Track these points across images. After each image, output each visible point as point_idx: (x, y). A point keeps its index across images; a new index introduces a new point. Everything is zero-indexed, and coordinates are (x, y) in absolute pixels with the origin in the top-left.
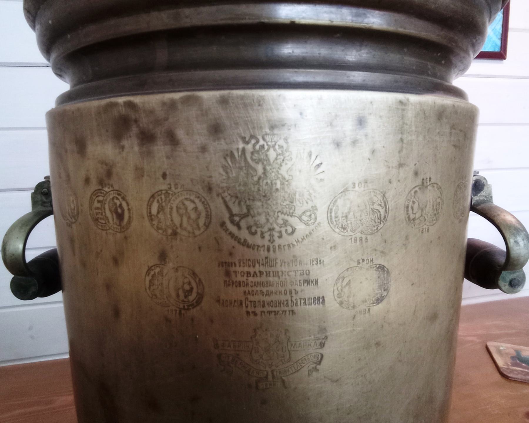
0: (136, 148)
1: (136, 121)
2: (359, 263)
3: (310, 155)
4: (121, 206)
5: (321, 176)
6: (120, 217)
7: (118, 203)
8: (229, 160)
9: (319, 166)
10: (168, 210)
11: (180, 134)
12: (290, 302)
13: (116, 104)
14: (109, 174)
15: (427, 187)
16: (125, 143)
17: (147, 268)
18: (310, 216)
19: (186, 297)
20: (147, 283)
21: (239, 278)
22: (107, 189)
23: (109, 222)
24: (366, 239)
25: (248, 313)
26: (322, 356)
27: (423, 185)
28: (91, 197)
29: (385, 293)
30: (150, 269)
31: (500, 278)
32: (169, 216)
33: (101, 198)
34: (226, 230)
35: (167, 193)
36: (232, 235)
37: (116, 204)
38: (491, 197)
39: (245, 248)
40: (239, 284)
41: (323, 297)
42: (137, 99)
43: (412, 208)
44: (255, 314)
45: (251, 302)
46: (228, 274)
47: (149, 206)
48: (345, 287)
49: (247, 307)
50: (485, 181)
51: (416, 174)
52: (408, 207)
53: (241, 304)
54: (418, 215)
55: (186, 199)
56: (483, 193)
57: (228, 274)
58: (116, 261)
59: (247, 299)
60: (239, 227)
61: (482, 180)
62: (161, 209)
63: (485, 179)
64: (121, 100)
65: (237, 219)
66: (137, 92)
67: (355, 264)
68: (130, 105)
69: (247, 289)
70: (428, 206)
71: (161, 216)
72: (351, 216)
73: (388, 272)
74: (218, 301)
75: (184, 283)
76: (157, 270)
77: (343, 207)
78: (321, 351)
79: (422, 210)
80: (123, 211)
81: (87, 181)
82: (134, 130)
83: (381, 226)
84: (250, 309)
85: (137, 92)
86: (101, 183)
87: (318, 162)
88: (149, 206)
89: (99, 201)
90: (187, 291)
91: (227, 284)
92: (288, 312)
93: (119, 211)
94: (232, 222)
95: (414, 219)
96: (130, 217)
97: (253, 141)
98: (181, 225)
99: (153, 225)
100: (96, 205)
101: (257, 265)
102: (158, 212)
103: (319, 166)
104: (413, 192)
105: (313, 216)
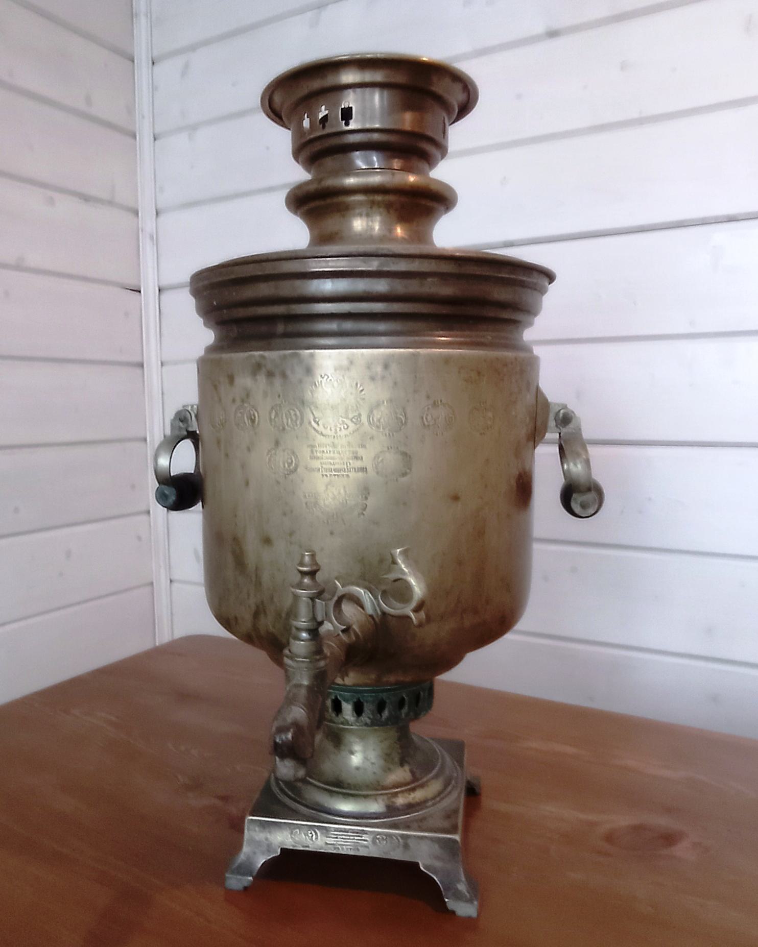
0: (264, 381)
1: (265, 366)
2: (388, 449)
3: (357, 384)
4: (254, 415)
5: (364, 397)
6: (253, 421)
7: (252, 413)
8: (313, 387)
9: (362, 391)
10: (280, 415)
11: (288, 372)
12: (346, 469)
13: (253, 356)
14: (248, 395)
15: (438, 406)
16: (258, 377)
17: (267, 451)
18: (357, 419)
19: (289, 466)
20: (267, 460)
21: (319, 455)
22: (246, 405)
23: (246, 425)
24: (393, 434)
25: (323, 475)
26: (366, 505)
27: (435, 404)
28: (236, 411)
29: (408, 471)
30: (269, 451)
31: (572, 500)
32: (281, 419)
33: (242, 411)
34: (312, 426)
35: (280, 406)
36: (315, 429)
37: (250, 414)
38: (580, 429)
39: (322, 437)
40: (318, 458)
41: (366, 469)
42: (266, 354)
43: (426, 419)
44: (326, 475)
45: (324, 468)
46: (312, 452)
47: (270, 413)
48: (380, 462)
49: (322, 472)
50: (573, 414)
51: (428, 397)
52: (422, 418)
53: (319, 470)
54: (431, 423)
55: (291, 409)
56: (571, 426)
57: (312, 452)
58: (249, 449)
59: (322, 467)
60: (318, 425)
61: (570, 413)
62: (277, 415)
63: (573, 412)
64: (257, 353)
65: (317, 420)
66: (286, 790)
67: (386, 449)
68: (263, 357)
69: (322, 461)
70: (440, 419)
71: (277, 419)
72: (382, 420)
73: (410, 457)
74: (306, 468)
75: (288, 459)
76: (273, 452)
77: (377, 415)
78: (365, 502)
79: (435, 420)
80: (255, 417)
81: (234, 401)
82: (264, 370)
83: (403, 427)
84: (324, 473)
85: (286, 790)
86: (243, 401)
87: (361, 388)
88: (270, 413)
89: (241, 413)
90: (290, 463)
91: (311, 458)
92: (345, 476)
93: (253, 417)
94: (315, 421)
95: (429, 426)
96: (259, 421)
97: (326, 377)
98: (287, 424)
99: (271, 424)
100: (239, 415)
101: (328, 447)
102: (275, 417)
103: (362, 391)
104: (426, 408)
105: (359, 419)
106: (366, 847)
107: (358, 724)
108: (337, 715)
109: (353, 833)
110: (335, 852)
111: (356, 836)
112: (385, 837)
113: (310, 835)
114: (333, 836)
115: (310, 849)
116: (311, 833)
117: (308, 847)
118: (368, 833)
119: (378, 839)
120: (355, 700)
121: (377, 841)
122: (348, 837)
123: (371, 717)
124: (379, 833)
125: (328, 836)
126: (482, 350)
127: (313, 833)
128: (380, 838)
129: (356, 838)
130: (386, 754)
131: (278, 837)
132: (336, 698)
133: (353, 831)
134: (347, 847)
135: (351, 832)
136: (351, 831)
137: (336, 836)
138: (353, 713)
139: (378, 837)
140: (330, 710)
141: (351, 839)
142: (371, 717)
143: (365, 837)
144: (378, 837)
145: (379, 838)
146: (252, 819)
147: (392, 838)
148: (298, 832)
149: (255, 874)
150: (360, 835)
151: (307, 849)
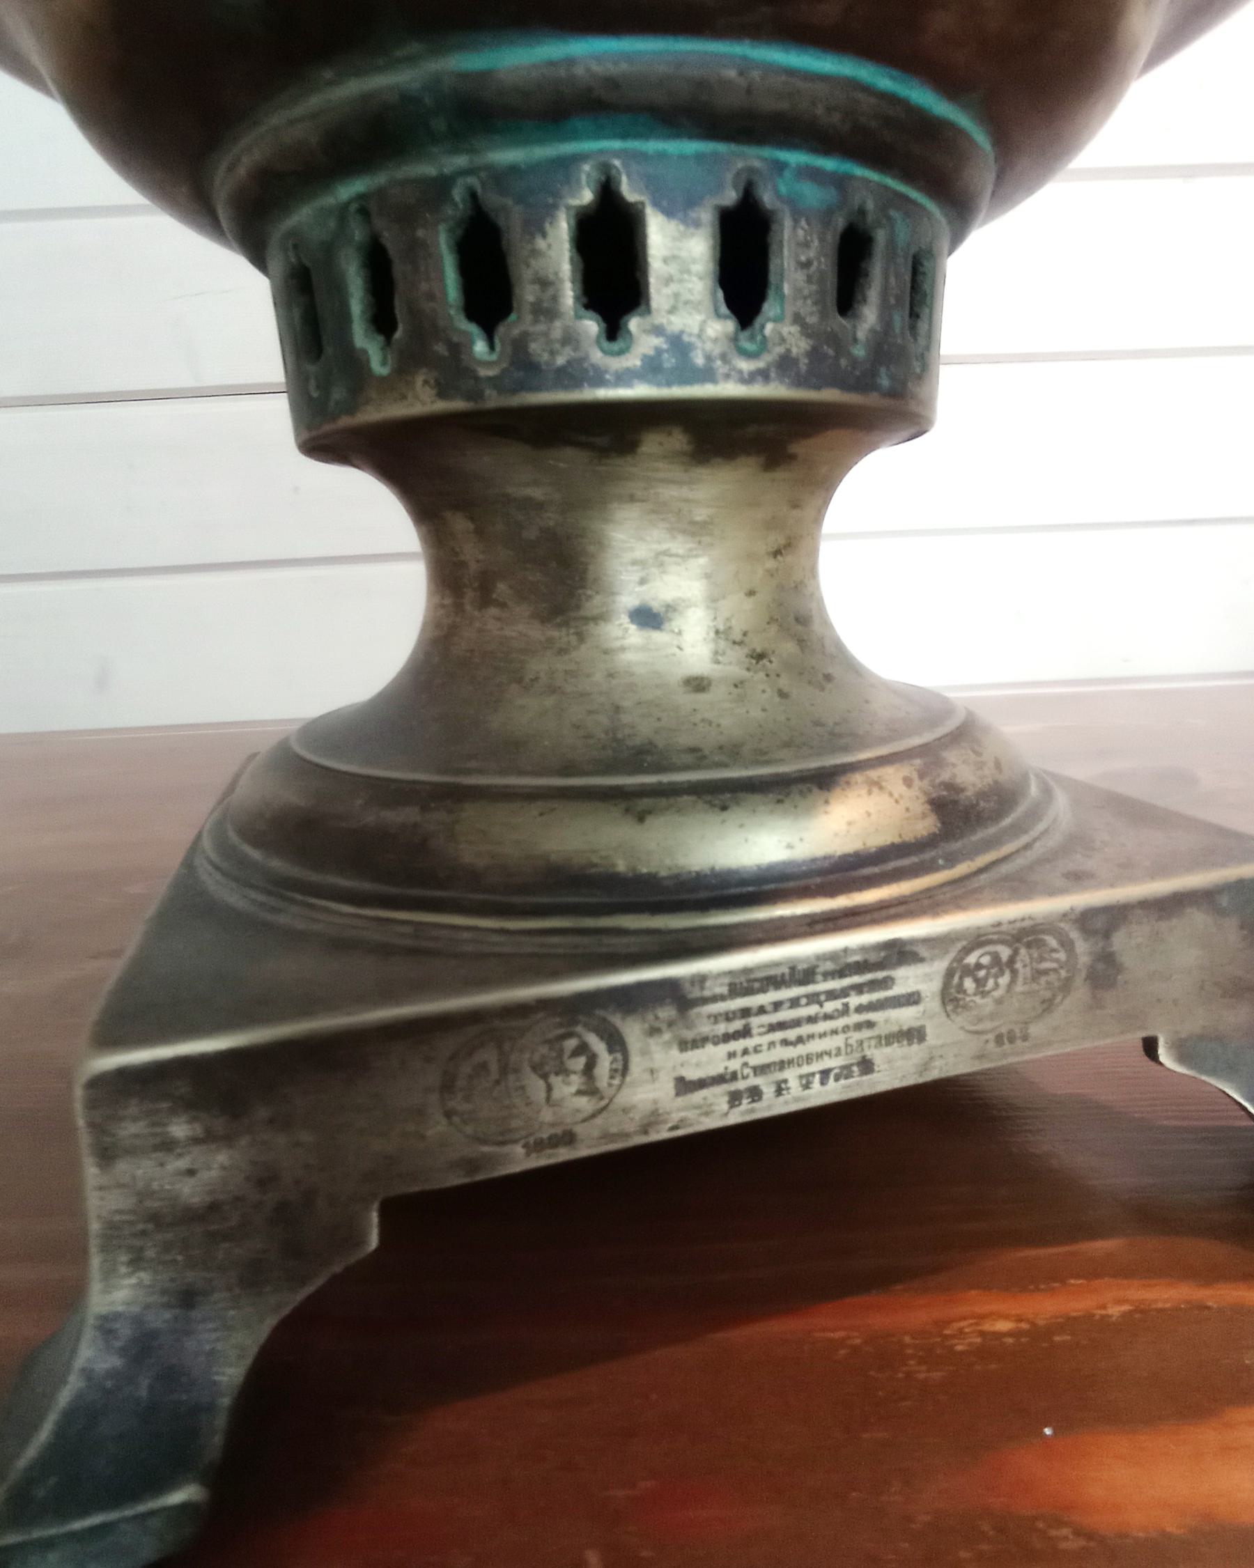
106: (914, 1035)
107: (745, 366)
108: (613, 331)
109: (841, 973)
110: (736, 1117)
111: (859, 989)
112: (1005, 952)
113: (581, 1062)
114: (722, 1028)
115: (583, 1151)
116: (583, 1049)
117: (569, 1138)
118: (923, 951)
119: (969, 971)
120: (730, 197)
121: (969, 984)
122: (813, 1010)
123: (812, 320)
124: (978, 939)
125: (689, 1035)
126: (573, 271)
127: (598, 1045)
128: (985, 960)
129: (854, 1000)
130: (89, 1359)
131: (361, 801)
132: (607, 191)
133: (843, 966)
134: (806, 1069)
135: (828, 975)
136: (829, 966)
137: (738, 1025)
138: (714, 294)
139: (971, 959)
140: (568, 295)
141: (827, 1017)
142: (812, 320)
143: (907, 979)
144: (971, 959)
145: (979, 966)
146: (123, 1074)
147: (1039, 944)
148: (494, 1067)
149: (215, 1441)
150: (880, 975)
151: (564, 1155)
